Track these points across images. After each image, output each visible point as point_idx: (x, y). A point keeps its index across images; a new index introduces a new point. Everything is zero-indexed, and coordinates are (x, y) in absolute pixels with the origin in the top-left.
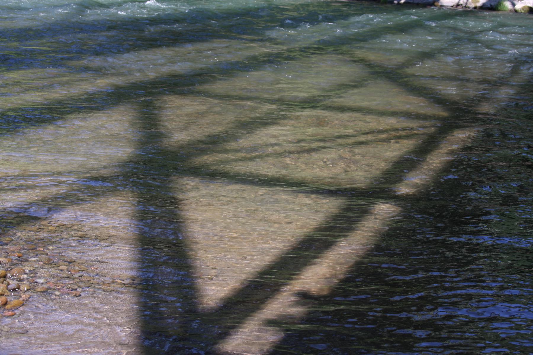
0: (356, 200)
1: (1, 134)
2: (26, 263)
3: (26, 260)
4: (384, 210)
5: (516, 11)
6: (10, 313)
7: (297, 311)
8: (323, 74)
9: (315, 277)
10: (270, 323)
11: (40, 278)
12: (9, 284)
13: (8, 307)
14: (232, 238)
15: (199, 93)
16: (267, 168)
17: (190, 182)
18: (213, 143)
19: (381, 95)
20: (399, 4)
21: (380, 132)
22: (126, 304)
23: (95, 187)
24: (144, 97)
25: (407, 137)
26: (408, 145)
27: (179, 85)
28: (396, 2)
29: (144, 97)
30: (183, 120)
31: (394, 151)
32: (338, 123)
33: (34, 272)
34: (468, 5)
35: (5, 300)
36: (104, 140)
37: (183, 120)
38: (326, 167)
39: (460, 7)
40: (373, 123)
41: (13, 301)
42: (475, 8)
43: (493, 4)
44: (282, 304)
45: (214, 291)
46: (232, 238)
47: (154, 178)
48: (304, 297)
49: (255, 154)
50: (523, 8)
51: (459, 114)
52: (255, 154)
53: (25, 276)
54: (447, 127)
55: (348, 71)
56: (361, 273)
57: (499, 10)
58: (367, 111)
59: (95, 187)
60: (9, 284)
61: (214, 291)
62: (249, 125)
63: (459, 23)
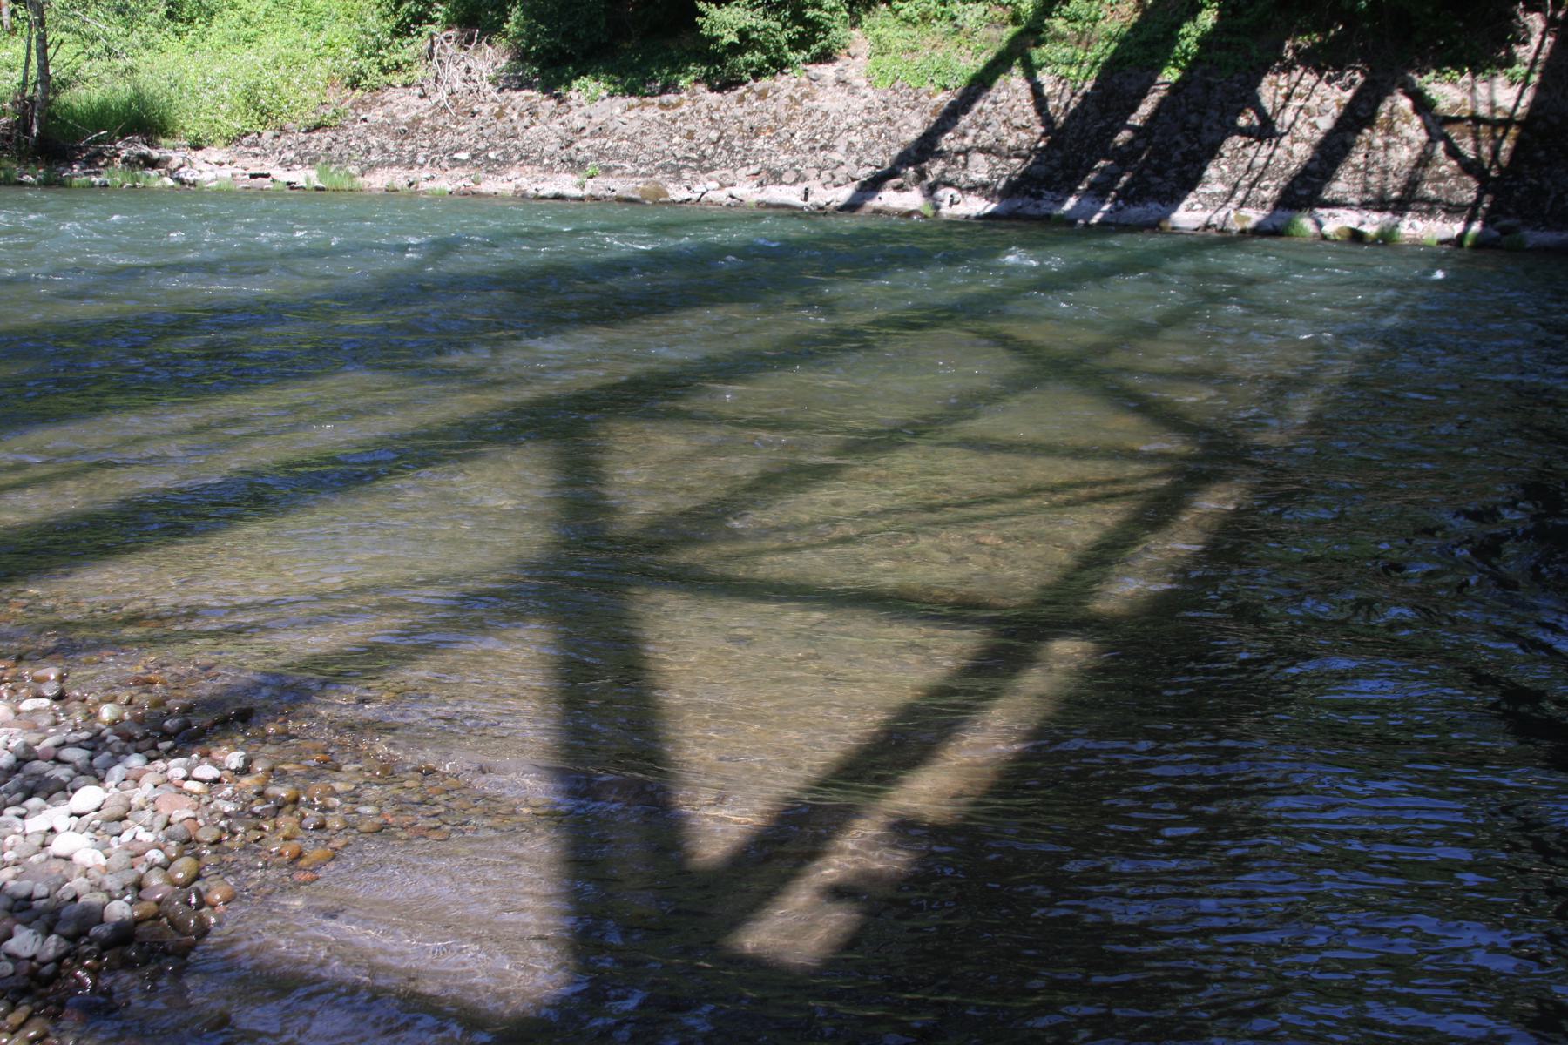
0: (1013, 635)
1: (8, 182)
2: (338, 775)
3: (338, 769)
4: (1068, 651)
5: (1324, 238)
6: (308, 875)
7: (891, 862)
8: (951, 367)
9: (927, 791)
10: (837, 893)
11: (366, 804)
12: (303, 817)
13: (303, 863)
14: (756, 714)
15: (688, 416)
16: (817, 566)
17: (671, 601)
18: (708, 520)
19: (1067, 414)
20: (1087, 225)
21: (1094, 484)
22: (541, 847)
23: (478, 608)
24: (566, 427)
25: (1111, 497)
26: (1109, 516)
27: (649, 396)
28: (1081, 222)
29: (566, 427)
30: (647, 473)
31: (1083, 528)
32: (961, 472)
33: (354, 797)
34: (1229, 226)
35: (296, 851)
36: (498, 509)
37: (647, 473)
38: (935, 563)
39: (1211, 232)
40: (1038, 470)
41: (314, 853)
42: (1243, 231)
43: (1278, 223)
44: (858, 850)
45: (721, 822)
46: (756, 714)
47: (592, 590)
48: (904, 829)
49: (790, 537)
50: (1339, 232)
51: (1217, 453)
52: (790, 537)
53: (337, 801)
54: (1191, 478)
55: (982, 368)
56: (1012, 781)
57: (1291, 235)
58: (1036, 449)
59: (478, 608)
60: (303, 817)
61: (721, 822)
62: (769, 484)
63: (1212, 260)
